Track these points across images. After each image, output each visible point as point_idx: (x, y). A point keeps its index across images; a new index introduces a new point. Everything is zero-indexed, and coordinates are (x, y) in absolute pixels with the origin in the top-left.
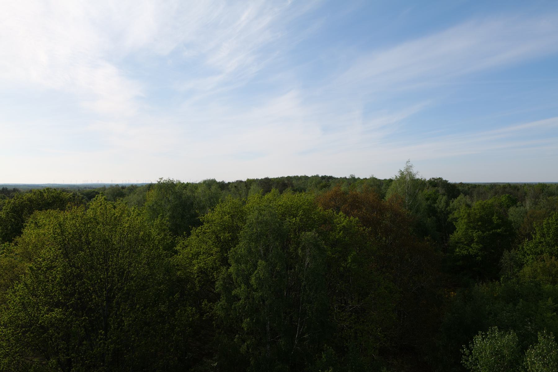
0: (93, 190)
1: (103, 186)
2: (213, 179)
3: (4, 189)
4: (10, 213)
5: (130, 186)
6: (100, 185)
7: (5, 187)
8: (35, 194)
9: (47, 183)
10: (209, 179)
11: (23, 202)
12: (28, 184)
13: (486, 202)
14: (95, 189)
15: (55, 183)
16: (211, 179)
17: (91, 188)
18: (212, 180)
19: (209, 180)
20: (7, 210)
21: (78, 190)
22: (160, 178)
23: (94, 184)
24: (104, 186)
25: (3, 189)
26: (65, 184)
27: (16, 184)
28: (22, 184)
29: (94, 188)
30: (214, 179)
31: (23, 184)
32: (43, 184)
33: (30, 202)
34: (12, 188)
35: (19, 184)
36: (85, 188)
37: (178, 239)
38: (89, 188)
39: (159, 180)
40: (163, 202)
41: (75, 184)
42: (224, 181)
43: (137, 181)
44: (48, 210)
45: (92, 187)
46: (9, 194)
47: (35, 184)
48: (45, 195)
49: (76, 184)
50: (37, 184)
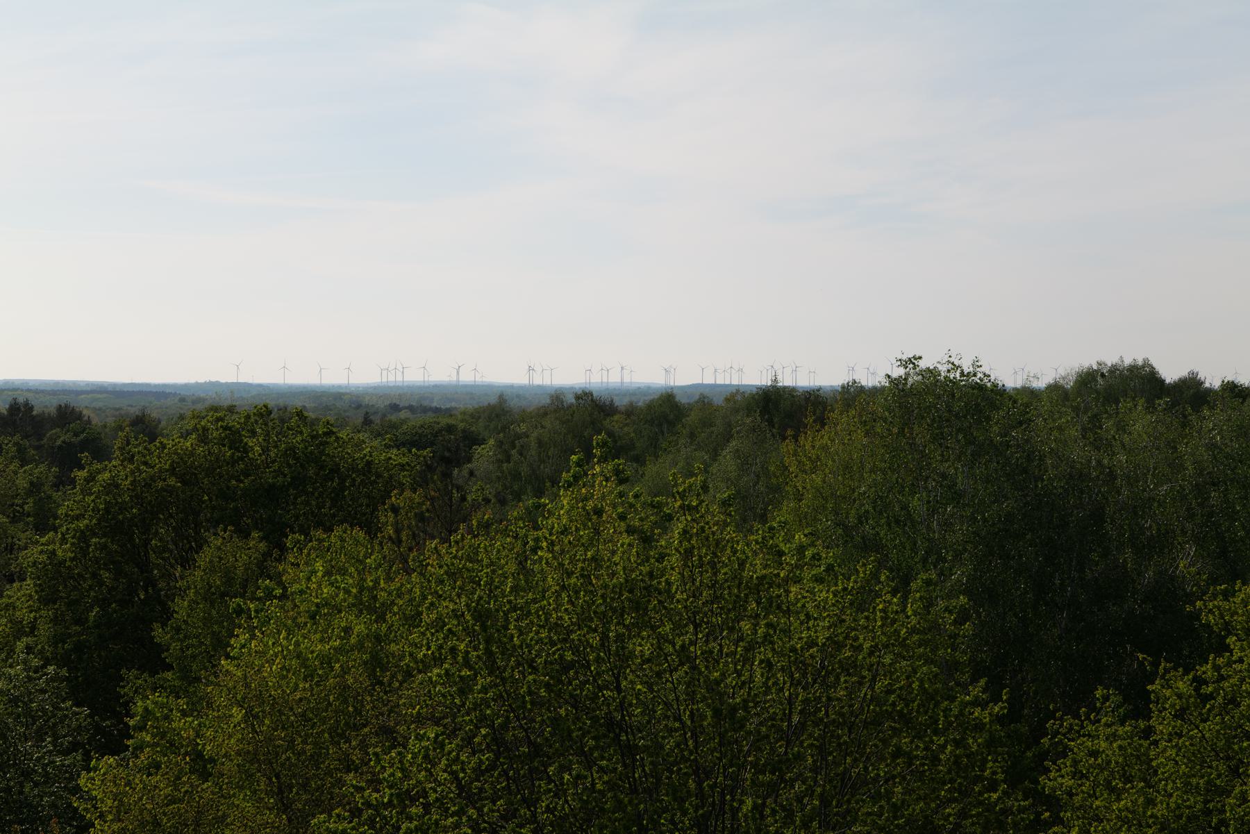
0: (444, 421)
1: (493, 400)
2: (1140, 363)
3: (19, 409)
4: (94, 535)
5: (571, 399)
6: (470, 391)
7: (21, 400)
8: (204, 438)
9: (201, 380)
10: (1110, 359)
11: (152, 478)
12: (115, 385)
13: (223, 416)
14: (449, 412)
15: (241, 380)
16: (1128, 361)
17: (425, 410)
18: (1133, 369)
19: (1114, 369)
20: (78, 518)
21: (360, 420)
22: (904, 357)
23: (436, 386)
24: (501, 396)
25: (15, 408)
26: (291, 387)
27: (57, 383)
28: (88, 384)
29: (437, 410)
30: (1147, 364)
31: (93, 384)
32: (186, 386)
33: (184, 482)
34: (49, 406)
35: (74, 383)
36: (395, 408)
37: (1061, 726)
38: (411, 408)
39: (898, 372)
40: (916, 503)
41: (340, 386)
42: (1201, 376)
43: (530, 369)
44: (338, 531)
45: (426, 403)
46: (40, 438)
47: (148, 385)
48: (254, 445)
49: (347, 386)
50: (155, 386)
